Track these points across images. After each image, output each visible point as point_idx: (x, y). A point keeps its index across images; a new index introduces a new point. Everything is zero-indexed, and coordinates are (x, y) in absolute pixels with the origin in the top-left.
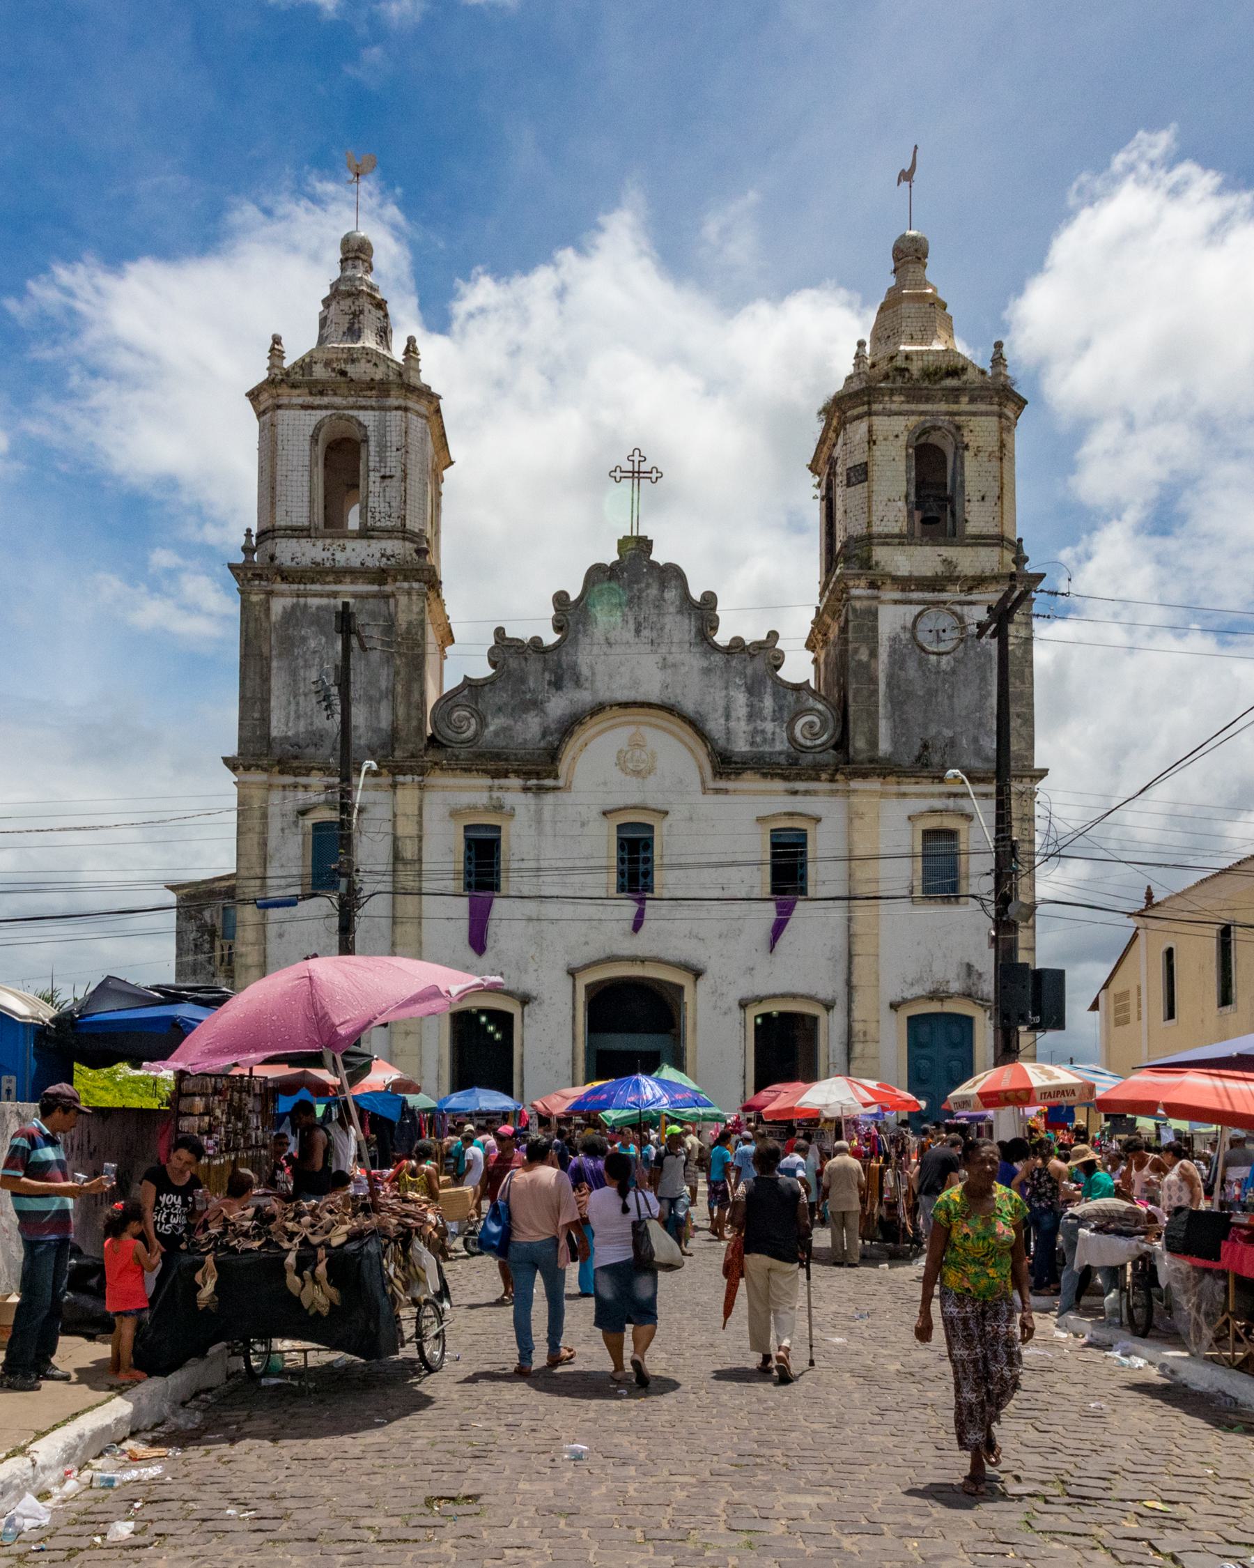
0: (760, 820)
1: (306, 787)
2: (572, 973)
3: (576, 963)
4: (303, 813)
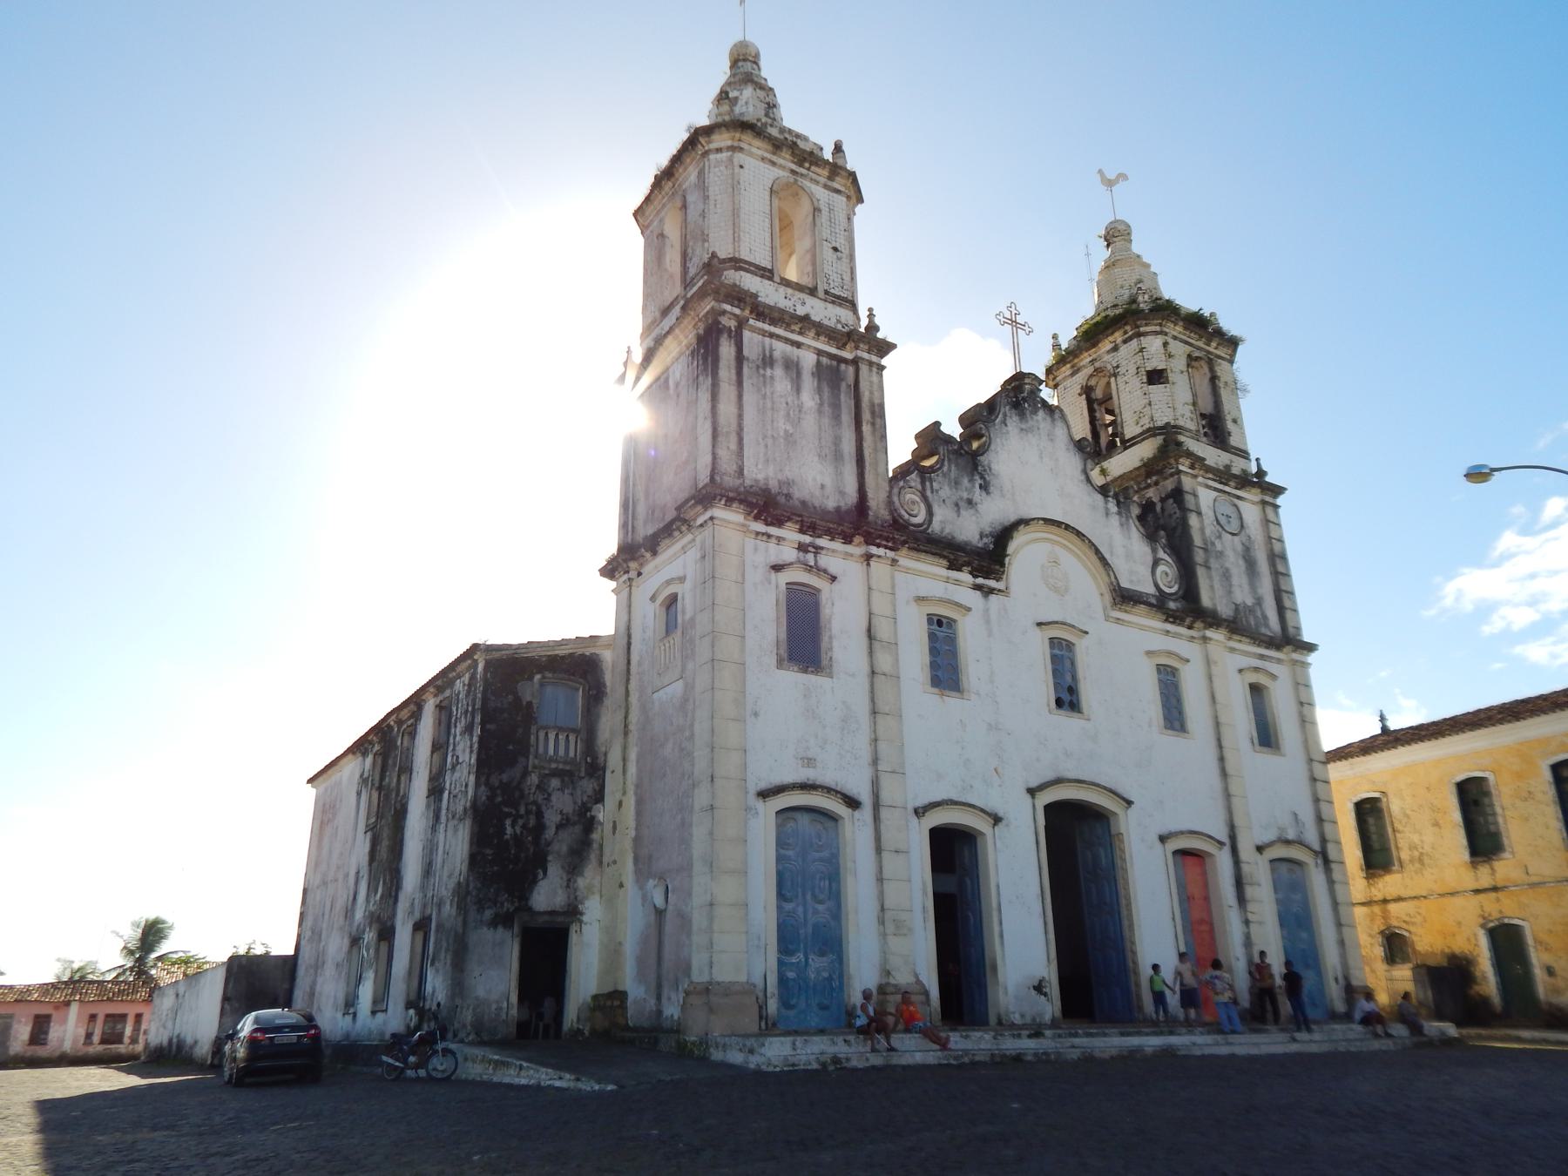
0: (1149, 653)
1: (779, 539)
2: (1032, 792)
3: (1034, 784)
4: (777, 568)
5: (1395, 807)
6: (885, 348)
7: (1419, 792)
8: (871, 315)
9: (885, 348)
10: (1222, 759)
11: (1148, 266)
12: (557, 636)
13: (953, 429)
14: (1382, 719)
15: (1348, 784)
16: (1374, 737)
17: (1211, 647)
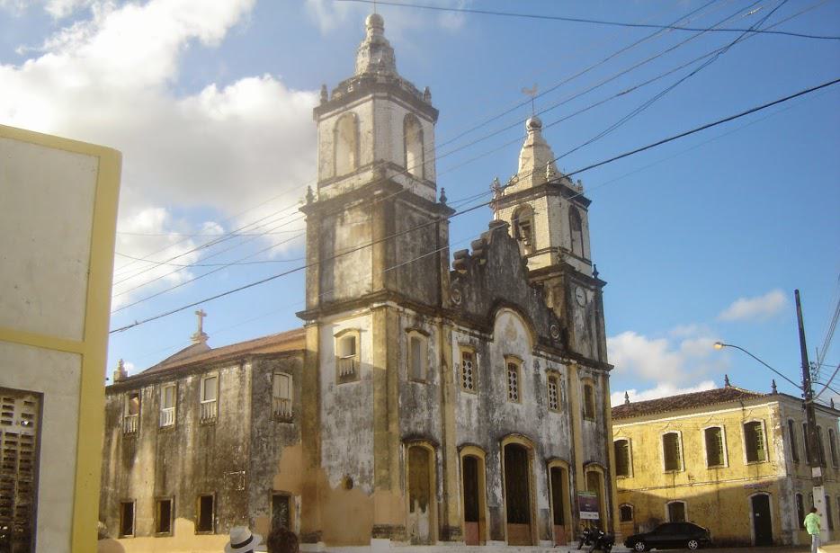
17: (572, 367)
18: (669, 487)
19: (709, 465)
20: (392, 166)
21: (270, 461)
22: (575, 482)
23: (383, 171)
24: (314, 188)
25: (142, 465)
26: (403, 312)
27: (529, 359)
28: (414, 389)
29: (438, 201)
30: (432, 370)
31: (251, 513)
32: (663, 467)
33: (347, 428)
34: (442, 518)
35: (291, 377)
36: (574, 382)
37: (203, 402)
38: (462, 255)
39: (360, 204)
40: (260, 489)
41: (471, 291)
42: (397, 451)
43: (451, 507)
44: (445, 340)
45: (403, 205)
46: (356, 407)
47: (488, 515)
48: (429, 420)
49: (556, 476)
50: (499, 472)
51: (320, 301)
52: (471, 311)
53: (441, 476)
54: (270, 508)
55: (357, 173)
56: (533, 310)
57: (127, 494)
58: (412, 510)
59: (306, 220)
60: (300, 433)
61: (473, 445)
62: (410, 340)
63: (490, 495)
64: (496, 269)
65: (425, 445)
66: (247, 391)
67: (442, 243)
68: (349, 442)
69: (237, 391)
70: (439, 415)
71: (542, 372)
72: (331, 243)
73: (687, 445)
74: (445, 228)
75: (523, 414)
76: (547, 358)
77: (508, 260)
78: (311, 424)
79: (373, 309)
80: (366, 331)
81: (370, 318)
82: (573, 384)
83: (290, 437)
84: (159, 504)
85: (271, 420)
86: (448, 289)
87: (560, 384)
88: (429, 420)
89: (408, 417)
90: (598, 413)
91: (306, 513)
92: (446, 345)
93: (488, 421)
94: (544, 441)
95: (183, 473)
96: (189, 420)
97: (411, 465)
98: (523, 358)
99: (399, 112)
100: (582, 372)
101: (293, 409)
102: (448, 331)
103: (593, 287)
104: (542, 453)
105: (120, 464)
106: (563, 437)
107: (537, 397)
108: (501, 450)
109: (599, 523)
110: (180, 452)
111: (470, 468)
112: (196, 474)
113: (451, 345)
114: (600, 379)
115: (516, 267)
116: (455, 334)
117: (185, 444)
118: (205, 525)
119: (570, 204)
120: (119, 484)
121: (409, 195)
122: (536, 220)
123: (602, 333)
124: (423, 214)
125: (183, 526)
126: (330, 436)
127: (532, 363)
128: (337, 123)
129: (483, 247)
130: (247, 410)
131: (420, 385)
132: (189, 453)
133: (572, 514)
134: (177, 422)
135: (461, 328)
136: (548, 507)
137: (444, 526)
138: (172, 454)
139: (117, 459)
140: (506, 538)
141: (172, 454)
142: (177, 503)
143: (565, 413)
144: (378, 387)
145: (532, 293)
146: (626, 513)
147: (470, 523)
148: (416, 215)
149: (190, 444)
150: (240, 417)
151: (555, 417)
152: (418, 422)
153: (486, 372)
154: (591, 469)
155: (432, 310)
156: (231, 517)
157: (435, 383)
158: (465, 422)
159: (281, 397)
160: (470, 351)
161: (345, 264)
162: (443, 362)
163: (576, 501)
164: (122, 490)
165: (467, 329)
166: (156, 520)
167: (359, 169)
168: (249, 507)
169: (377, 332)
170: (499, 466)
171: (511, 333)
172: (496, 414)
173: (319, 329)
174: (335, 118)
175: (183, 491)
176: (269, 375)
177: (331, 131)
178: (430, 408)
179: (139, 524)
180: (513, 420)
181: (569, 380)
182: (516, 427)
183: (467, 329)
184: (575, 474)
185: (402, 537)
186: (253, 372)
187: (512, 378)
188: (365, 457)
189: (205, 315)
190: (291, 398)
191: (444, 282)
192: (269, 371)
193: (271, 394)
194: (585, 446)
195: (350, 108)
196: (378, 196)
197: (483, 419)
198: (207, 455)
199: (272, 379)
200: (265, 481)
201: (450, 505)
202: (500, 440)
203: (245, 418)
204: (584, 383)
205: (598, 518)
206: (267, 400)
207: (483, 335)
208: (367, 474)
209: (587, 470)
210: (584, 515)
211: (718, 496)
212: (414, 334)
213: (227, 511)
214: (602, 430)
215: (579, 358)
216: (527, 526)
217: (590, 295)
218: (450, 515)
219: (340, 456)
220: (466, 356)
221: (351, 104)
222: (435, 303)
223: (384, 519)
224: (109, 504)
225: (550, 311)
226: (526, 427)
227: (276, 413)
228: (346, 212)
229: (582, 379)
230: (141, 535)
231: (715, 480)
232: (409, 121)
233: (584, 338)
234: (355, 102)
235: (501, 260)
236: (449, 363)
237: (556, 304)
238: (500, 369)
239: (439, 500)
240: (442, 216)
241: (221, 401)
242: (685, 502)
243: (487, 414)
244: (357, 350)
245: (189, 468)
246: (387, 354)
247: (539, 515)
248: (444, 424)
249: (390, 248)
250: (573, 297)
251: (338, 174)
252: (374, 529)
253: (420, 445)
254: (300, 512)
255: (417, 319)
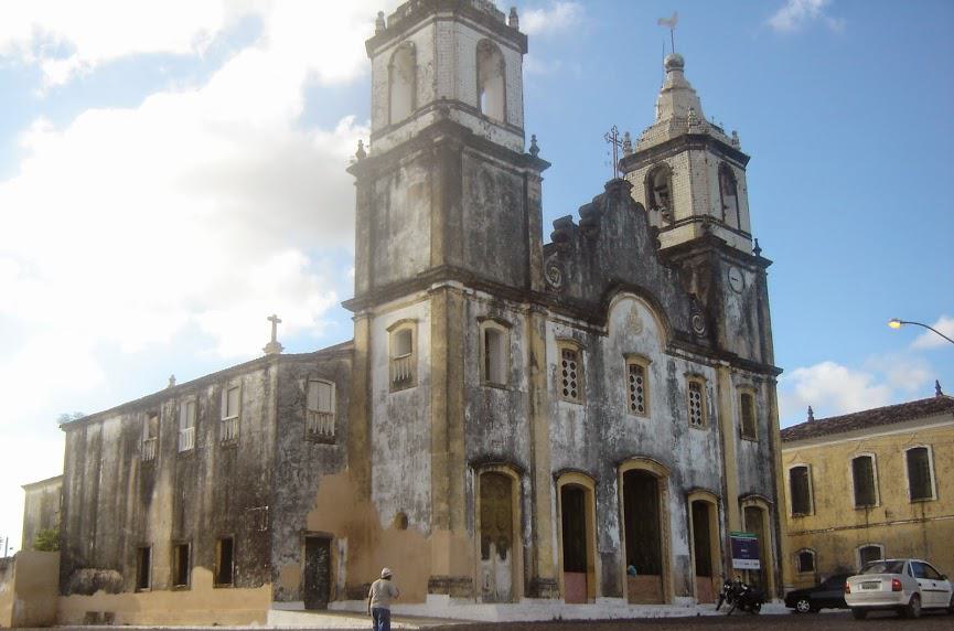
5: (817, 474)
6: (545, 165)
7: (830, 465)
8: (534, 139)
9: (545, 165)
10: (505, 107)
11: (694, 92)
12: (199, 377)
13: (577, 220)
14: (811, 412)
15: (790, 457)
16: (804, 425)
17: (722, 370)
18: (861, 527)
19: (912, 499)
20: (459, 105)
21: (302, 492)
22: (726, 520)
23: (445, 112)
24: (366, 142)
25: (160, 499)
26: (474, 296)
27: (660, 359)
28: (489, 397)
29: (527, 151)
30: (517, 372)
31: (275, 560)
32: (852, 500)
33: (401, 450)
34: (530, 565)
35: (334, 385)
36: (726, 392)
37: (223, 419)
38: (563, 225)
39: (418, 157)
40: (287, 530)
41: (576, 268)
42: (462, 480)
43: (543, 553)
44: (538, 333)
45: (472, 155)
46: (412, 421)
47: (598, 563)
48: (511, 438)
49: (700, 515)
50: (616, 506)
51: (371, 286)
52: (576, 296)
53: (528, 511)
54: (302, 554)
55: (415, 118)
56: (667, 297)
57: (144, 538)
58: (486, 556)
59: (355, 184)
60: (346, 457)
61: (577, 471)
62: (483, 332)
63: (602, 538)
64: (612, 241)
65: (506, 470)
66: (271, 404)
67: (532, 209)
68: (403, 467)
69: (261, 404)
70: (527, 431)
71: (679, 375)
72: (385, 211)
73: (884, 472)
74: (536, 187)
75: (651, 431)
76: (687, 358)
77: (630, 230)
78: (359, 445)
79: (431, 292)
80: (424, 321)
81: (427, 304)
82: (723, 391)
83: (332, 462)
84: (177, 550)
85: (304, 439)
86: (540, 266)
87: (705, 393)
88: (511, 438)
89: (481, 433)
90: (756, 424)
91: (353, 560)
92: (537, 338)
93: (600, 440)
94: (683, 466)
95: (202, 510)
96: (209, 443)
97: (483, 496)
98: (652, 358)
99: (470, 38)
100: (738, 377)
101: (336, 425)
102: (539, 321)
103: (753, 268)
104: (680, 482)
105: (138, 500)
106: (710, 461)
107: (673, 409)
108: (618, 477)
109: (762, 573)
110: (199, 483)
111: (573, 503)
112: (215, 512)
113: (543, 339)
114: (764, 387)
115: (642, 240)
116: (550, 325)
117: (204, 472)
118: (224, 578)
119: (720, 160)
120: (136, 525)
121: (482, 143)
122: (675, 182)
123: (766, 326)
124: (503, 168)
125: (201, 576)
126: (382, 460)
127: (665, 366)
128: (393, 57)
129: (593, 213)
130: (270, 428)
131: (499, 392)
132: (209, 483)
133: (723, 562)
134: (196, 445)
135: (559, 317)
136: (686, 553)
137: (533, 579)
138: (190, 488)
139: (135, 492)
140: (625, 593)
141: (190, 488)
142: (196, 549)
143: (714, 430)
144: (437, 394)
145: (666, 274)
146: (806, 561)
147: (573, 575)
148: (495, 171)
149: (209, 473)
150: (264, 437)
151: (698, 437)
152: (495, 440)
153: (597, 376)
154: (751, 504)
155: (517, 293)
156: (252, 565)
157: (520, 389)
158: (566, 441)
159: (320, 410)
160: (574, 348)
161: (401, 236)
162: (533, 361)
163: (728, 546)
164: (139, 533)
165: (568, 320)
166: (173, 570)
167: (417, 112)
168: (274, 552)
169: (436, 322)
170: (615, 499)
171: (633, 325)
172: (612, 431)
173: (369, 322)
174: (391, 50)
175: (202, 533)
176: (301, 382)
177: (386, 68)
178: (512, 421)
179: (156, 575)
180: (636, 438)
181: (719, 387)
182: (640, 447)
183: (568, 320)
184: (726, 510)
185: (467, 592)
186: (279, 378)
187: (636, 384)
188: (422, 486)
189: (280, 321)
190: (333, 411)
191: (534, 257)
192: (302, 377)
193: (304, 406)
194: (741, 473)
195: (409, 35)
196: (438, 145)
197: (590, 436)
198: (227, 486)
199: (306, 387)
200: (295, 519)
201: (540, 550)
202: (618, 464)
203: (270, 437)
204: (741, 391)
205: (758, 567)
206: (299, 413)
207: (592, 327)
208: (424, 508)
209: (744, 505)
210: (738, 563)
211: (925, 536)
212: (490, 324)
213: (248, 559)
214: (766, 452)
215: (733, 359)
216: (658, 578)
217: (750, 278)
218: (540, 563)
219: (393, 485)
220: (566, 354)
221: (409, 31)
222: (522, 283)
223: (442, 568)
224: (126, 550)
225: (692, 297)
226: (655, 447)
227: (311, 431)
228: (403, 169)
229: (737, 387)
230: (158, 588)
231: (920, 517)
232: (485, 50)
233: (740, 333)
234: (412, 30)
235: (620, 230)
236: (540, 362)
237: (701, 289)
238: (617, 372)
239: (525, 542)
240: (532, 171)
241: (244, 416)
242: (882, 547)
243: (599, 431)
244: (414, 349)
245: (208, 502)
246: (448, 350)
247: (674, 564)
248: (533, 444)
249: (454, 211)
250: (725, 279)
251: (394, 122)
252: (430, 581)
253: (497, 473)
254: (345, 559)
255: (493, 304)
